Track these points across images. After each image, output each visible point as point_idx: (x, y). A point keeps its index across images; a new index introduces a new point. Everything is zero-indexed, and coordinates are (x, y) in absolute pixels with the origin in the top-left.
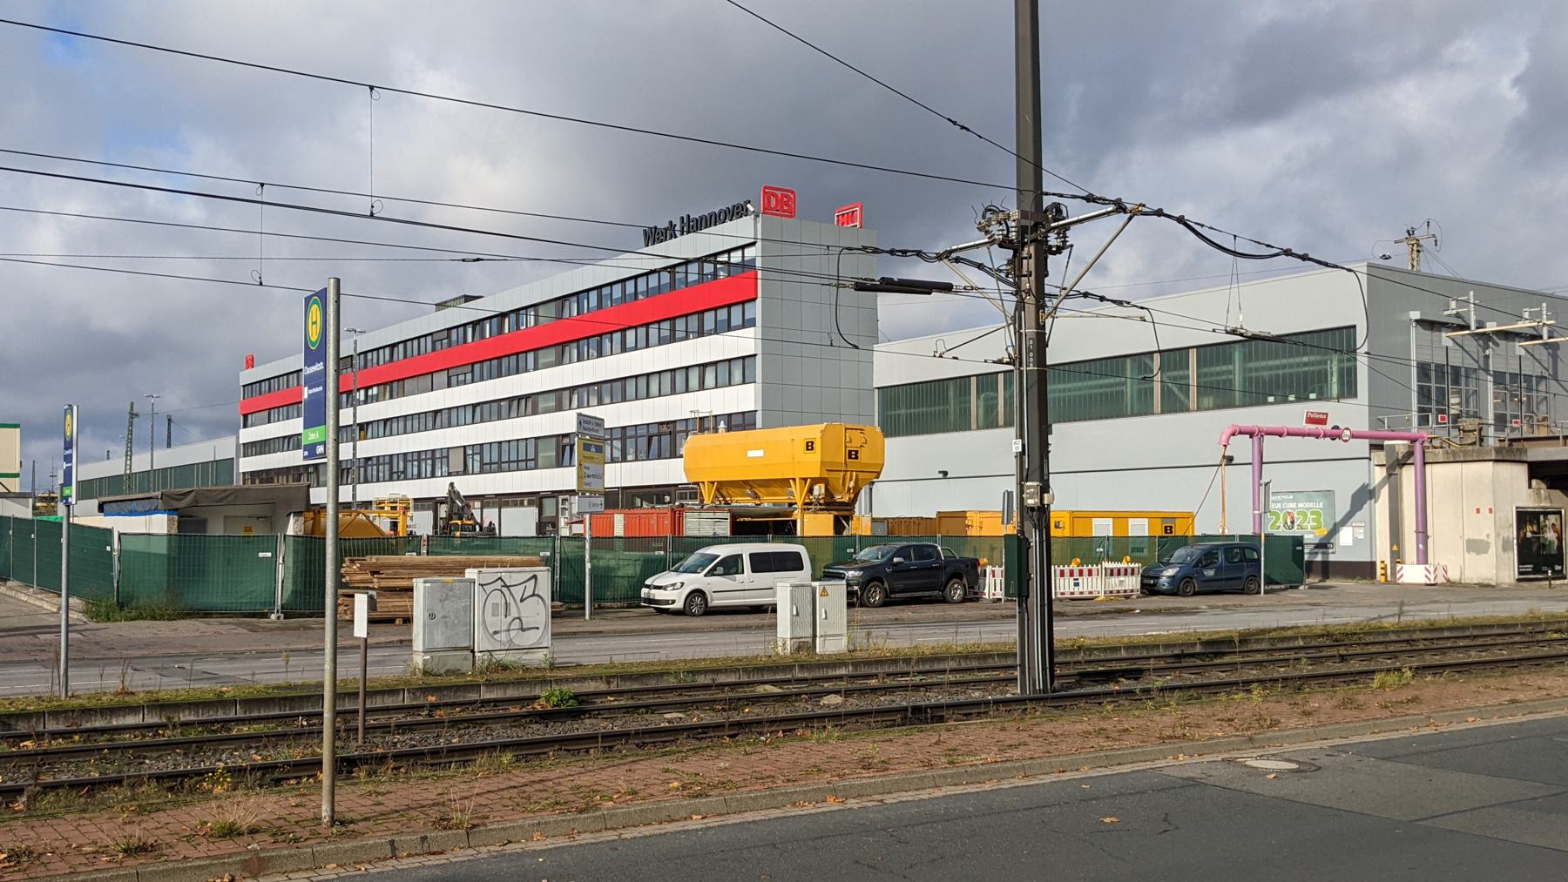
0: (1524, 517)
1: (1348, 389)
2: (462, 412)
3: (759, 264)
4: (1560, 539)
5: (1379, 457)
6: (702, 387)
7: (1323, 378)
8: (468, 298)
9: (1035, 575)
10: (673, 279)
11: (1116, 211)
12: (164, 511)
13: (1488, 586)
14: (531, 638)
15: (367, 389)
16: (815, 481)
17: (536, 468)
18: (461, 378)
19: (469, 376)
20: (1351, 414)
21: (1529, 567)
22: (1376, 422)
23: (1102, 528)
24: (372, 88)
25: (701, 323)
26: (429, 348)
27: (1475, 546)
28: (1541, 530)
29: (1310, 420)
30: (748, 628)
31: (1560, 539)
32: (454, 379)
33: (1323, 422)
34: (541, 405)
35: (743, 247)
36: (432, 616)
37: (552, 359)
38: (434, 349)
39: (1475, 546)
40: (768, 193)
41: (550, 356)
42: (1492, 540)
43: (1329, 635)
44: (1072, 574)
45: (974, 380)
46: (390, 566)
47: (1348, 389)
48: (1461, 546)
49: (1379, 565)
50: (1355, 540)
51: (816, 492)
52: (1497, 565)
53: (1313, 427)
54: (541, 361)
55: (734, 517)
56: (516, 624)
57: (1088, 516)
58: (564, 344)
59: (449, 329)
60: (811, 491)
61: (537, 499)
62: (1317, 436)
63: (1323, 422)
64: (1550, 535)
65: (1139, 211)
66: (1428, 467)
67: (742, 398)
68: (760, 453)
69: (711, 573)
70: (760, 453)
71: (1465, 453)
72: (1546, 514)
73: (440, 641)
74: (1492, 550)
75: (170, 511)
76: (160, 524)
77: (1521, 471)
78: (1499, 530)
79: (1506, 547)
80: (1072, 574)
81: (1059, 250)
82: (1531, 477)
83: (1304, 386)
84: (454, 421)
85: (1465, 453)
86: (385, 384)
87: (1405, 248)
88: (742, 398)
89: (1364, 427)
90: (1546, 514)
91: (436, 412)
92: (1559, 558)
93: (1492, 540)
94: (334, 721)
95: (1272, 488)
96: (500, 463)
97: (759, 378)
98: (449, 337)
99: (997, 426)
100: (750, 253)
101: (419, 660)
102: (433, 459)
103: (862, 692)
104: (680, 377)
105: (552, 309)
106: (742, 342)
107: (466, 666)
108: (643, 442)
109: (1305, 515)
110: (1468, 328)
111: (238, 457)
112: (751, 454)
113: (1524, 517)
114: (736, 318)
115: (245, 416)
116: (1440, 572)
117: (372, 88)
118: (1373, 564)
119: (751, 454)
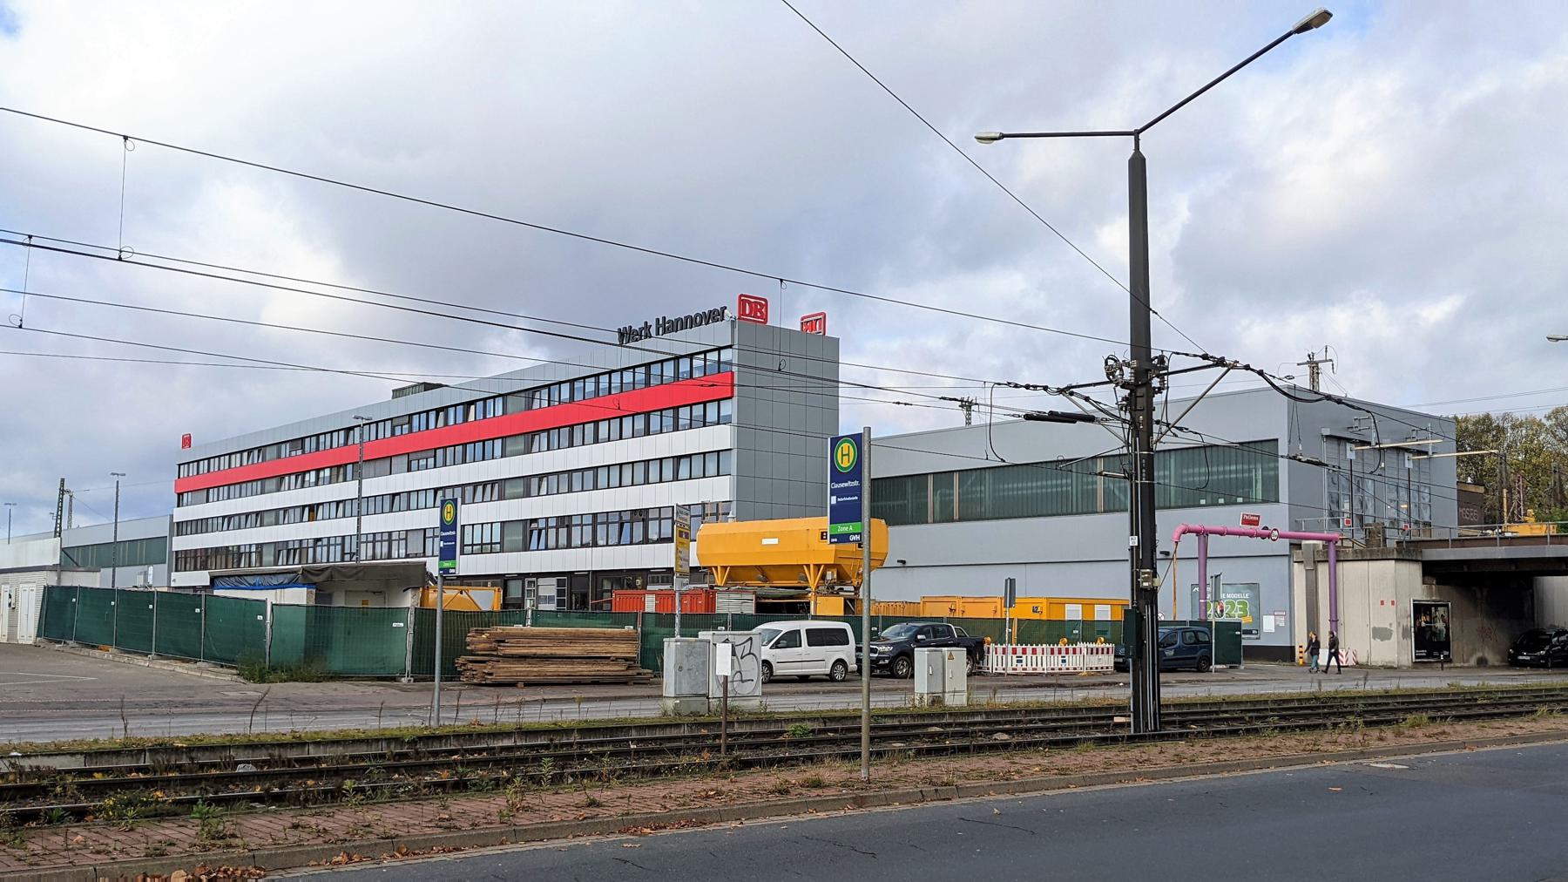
0: (1420, 609)
1: (1271, 496)
2: (422, 495)
3: (1283, 449)
4: (1447, 628)
5: (1298, 555)
6: (676, 478)
7: (1249, 483)
8: (428, 387)
9: (565, 668)
10: (648, 374)
11: (1216, 365)
12: (303, 585)
13: (1391, 668)
14: (747, 689)
15: (318, 471)
16: (828, 567)
17: (502, 551)
18: (423, 462)
19: (431, 461)
20: (1275, 516)
21: (1423, 652)
22: (1295, 524)
23: (1073, 612)
24: (126, 138)
25: (676, 418)
26: (388, 434)
27: (1381, 634)
28: (1433, 620)
29: (1246, 522)
30: (817, 693)
31: (1447, 628)
32: (414, 464)
33: (1256, 523)
34: (508, 491)
35: (719, 349)
36: (681, 668)
37: (521, 447)
38: (393, 434)
39: (1381, 634)
40: (743, 300)
41: (520, 444)
42: (1394, 628)
43: (1317, 699)
44: (1014, 651)
45: (930, 479)
46: (514, 636)
47: (1271, 496)
48: (1368, 633)
49: (1297, 650)
50: (1277, 627)
51: (829, 577)
52: (1398, 650)
53: (1247, 528)
54: (508, 449)
55: (757, 598)
56: (738, 677)
57: (1062, 603)
58: (534, 434)
59: (411, 416)
60: (823, 577)
61: (502, 581)
62: (1251, 536)
63: (1256, 523)
64: (1440, 625)
65: (1234, 366)
66: (1340, 565)
67: (719, 489)
68: (775, 541)
69: (776, 646)
70: (775, 541)
71: (1372, 552)
72: (1436, 606)
73: (686, 690)
74: (1394, 636)
75: (309, 585)
76: (299, 596)
77: (1415, 571)
78: (1397, 618)
79: (1405, 634)
80: (1014, 651)
81: (1160, 390)
82: (1424, 574)
83: (1232, 493)
84: (413, 505)
85: (1372, 552)
86: (339, 467)
87: (1306, 369)
88: (719, 489)
89: (1285, 530)
90: (1436, 606)
91: (394, 495)
92: (1446, 645)
93: (1394, 628)
94: (1534, 665)
95: (1222, 580)
96: (374, 542)
97: (734, 471)
98: (410, 422)
99: (953, 521)
100: (726, 355)
101: (670, 704)
102: (390, 541)
103: (1019, 731)
104: (654, 468)
105: (521, 402)
106: (720, 437)
107: (704, 710)
108: (614, 528)
109: (1233, 605)
110: (1369, 443)
111: (171, 536)
112: (765, 542)
113: (1420, 609)
114: (712, 415)
115: (180, 495)
116: (1351, 656)
117: (126, 138)
118: (1292, 649)
119: (765, 542)
